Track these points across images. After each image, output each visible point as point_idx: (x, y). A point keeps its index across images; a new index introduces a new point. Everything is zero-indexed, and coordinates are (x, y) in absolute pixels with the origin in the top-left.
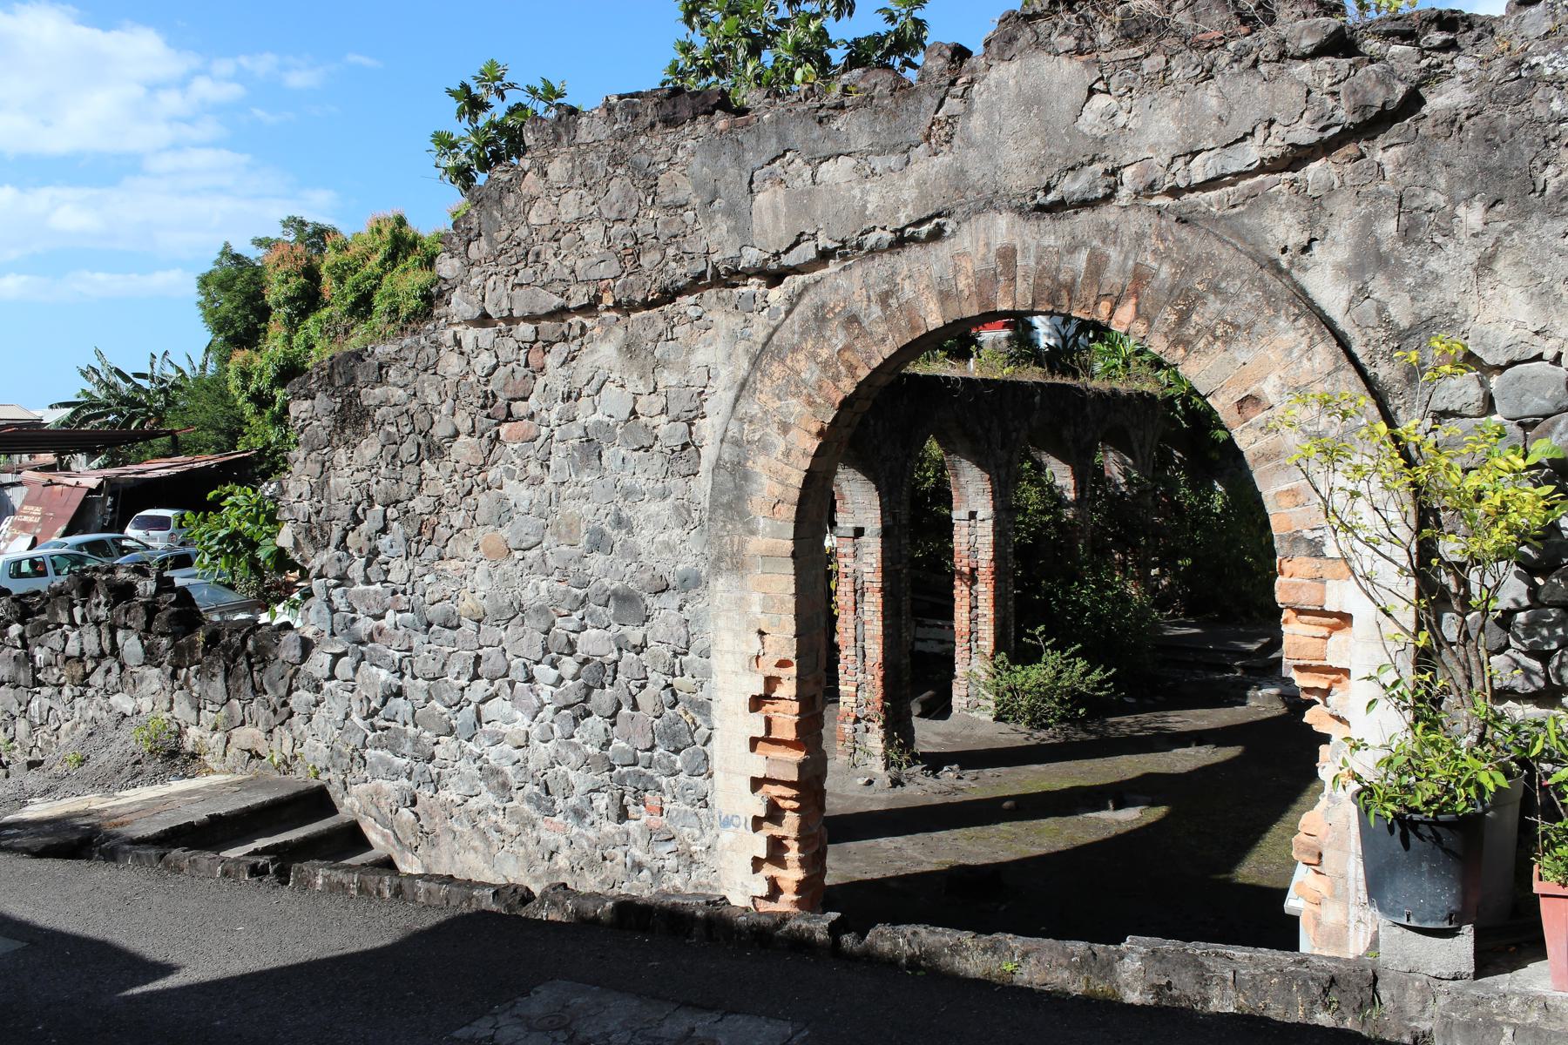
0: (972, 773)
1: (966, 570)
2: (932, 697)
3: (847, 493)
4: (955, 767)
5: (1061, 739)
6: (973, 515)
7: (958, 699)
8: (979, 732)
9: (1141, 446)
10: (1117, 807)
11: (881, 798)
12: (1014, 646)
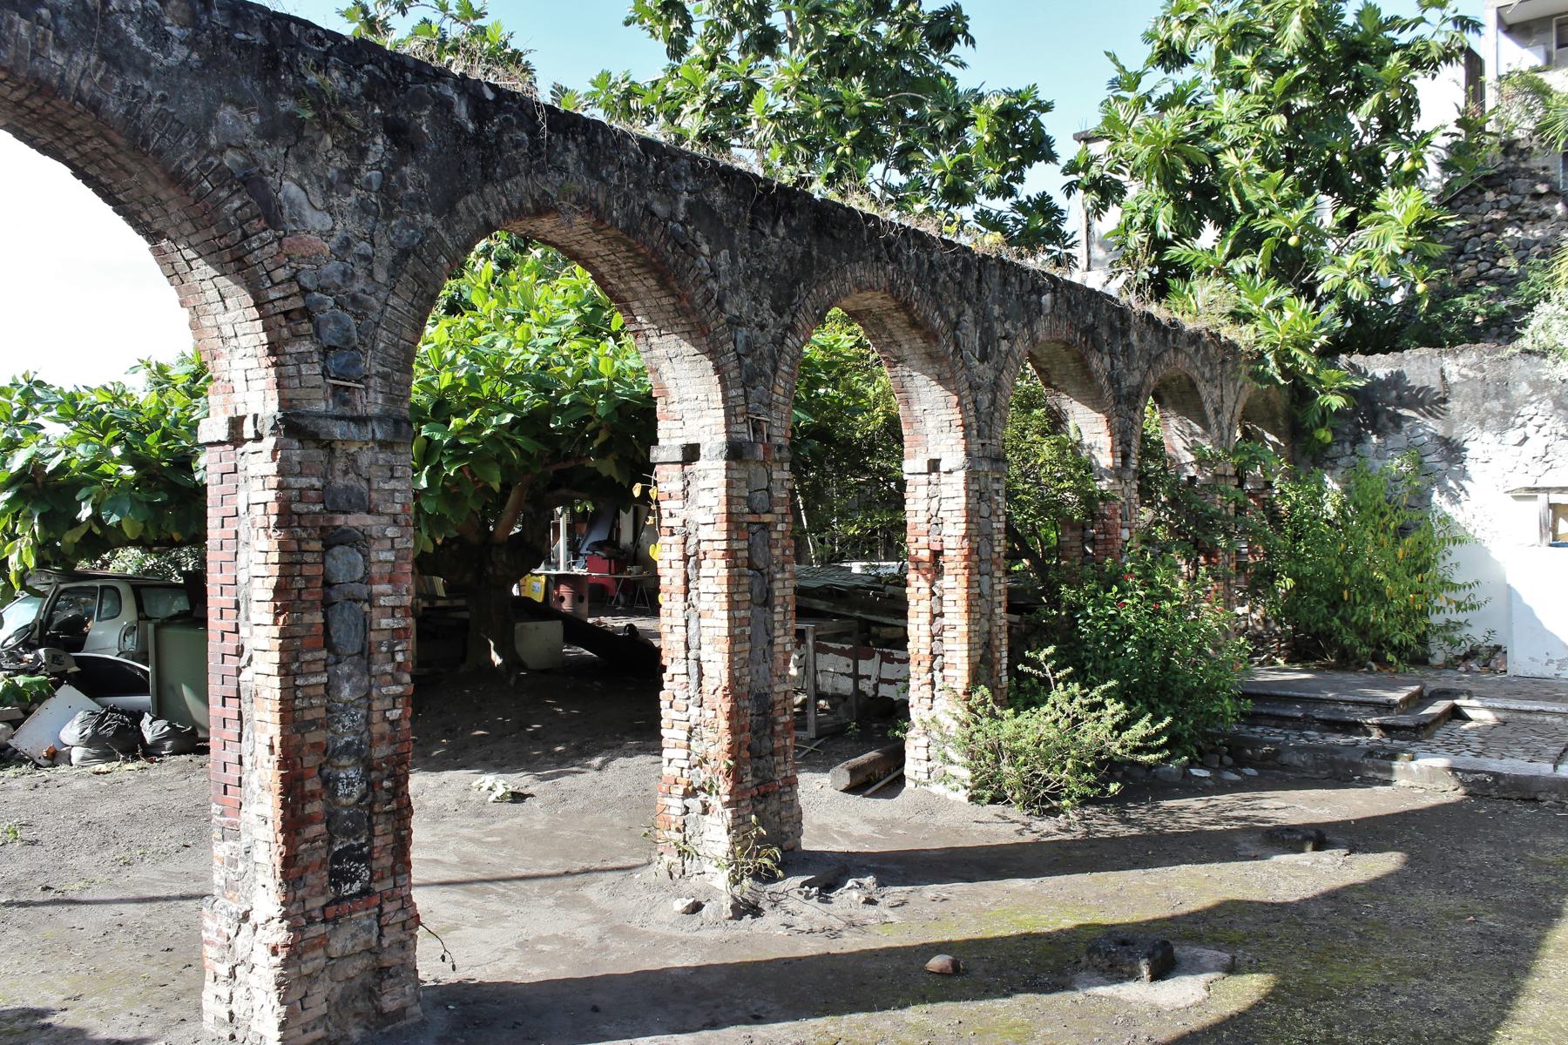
0: (897, 892)
1: (925, 555)
2: (873, 762)
3: (670, 384)
4: (869, 880)
5: (1079, 832)
6: (934, 465)
7: (913, 767)
8: (941, 819)
9: (1217, 412)
10: (1158, 975)
11: (715, 941)
12: (1006, 680)
